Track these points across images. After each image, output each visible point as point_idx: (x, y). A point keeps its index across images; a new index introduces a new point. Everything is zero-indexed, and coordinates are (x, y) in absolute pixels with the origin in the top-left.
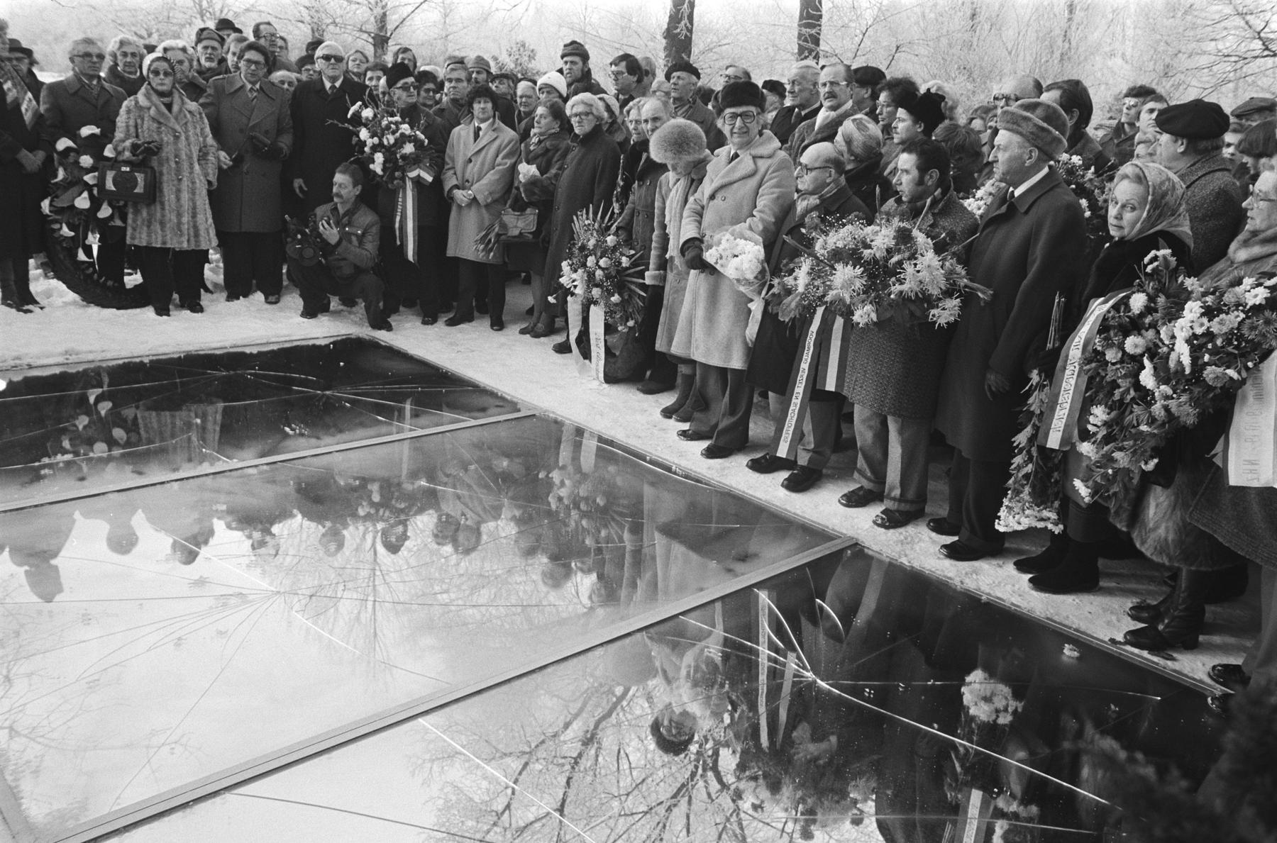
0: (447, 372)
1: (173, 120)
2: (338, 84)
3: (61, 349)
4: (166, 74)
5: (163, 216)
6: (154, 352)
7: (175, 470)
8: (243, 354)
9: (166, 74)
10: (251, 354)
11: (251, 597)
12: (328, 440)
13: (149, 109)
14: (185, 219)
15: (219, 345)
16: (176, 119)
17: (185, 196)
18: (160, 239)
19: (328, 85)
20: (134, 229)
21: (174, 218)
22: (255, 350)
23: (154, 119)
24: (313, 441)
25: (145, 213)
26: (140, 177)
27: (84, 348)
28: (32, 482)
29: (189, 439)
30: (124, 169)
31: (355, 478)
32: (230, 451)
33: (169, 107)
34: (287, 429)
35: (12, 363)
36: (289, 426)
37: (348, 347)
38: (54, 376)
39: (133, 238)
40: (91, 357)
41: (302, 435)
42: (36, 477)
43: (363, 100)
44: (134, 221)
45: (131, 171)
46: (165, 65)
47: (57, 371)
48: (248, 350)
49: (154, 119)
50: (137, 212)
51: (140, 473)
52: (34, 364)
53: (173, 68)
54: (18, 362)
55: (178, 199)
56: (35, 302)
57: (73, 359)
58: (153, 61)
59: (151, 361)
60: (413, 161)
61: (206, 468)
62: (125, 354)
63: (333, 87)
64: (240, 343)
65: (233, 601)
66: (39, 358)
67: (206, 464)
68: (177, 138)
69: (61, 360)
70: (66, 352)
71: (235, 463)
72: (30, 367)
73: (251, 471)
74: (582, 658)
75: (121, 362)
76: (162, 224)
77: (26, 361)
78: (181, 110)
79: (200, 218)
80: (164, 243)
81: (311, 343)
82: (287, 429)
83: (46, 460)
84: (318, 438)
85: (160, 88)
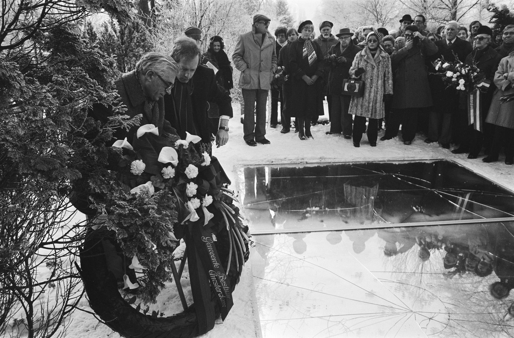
0: (496, 185)
1: (373, 61)
2: (453, 42)
3: (319, 157)
4: (374, 41)
5: (362, 103)
6: (354, 161)
7: (362, 223)
8: (392, 164)
9: (374, 41)
10: (396, 164)
11: (397, 311)
12: (435, 217)
13: (365, 56)
14: (371, 105)
15: (382, 160)
16: (375, 60)
17: (372, 95)
18: (360, 113)
19: (448, 42)
20: (351, 108)
21: (367, 104)
22: (397, 163)
23: (365, 61)
24: (427, 217)
25: (356, 101)
26: (357, 85)
27: (328, 156)
28: (302, 219)
29: (368, 206)
30: (352, 82)
31: (452, 244)
32: (386, 217)
33: (373, 55)
34: (414, 208)
35: (300, 161)
36: (416, 207)
37: (441, 165)
38: (315, 167)
39: (350, 111)
40: (329, 161)
41: (421, 212)
42: (304, 218)
43: (67, 138)
44: (352, 104)
45: (355, 83)
46: (374, 37)
47: (316, 165)
48: (394, 163)
49: (365, 61)
50: (353, 100)
51: (346, 222)
52: (308, 162)
53: (377, 38)
54: (303, 161)
55: (369, 95)
56: (311, 136)
57: (323, 161)
58: (370, 36)
59: (353, 165)
60: (478, 79)
61: (375, 225)
62: (343, 160)
63: (450, 43)
64: (391, 159)
65: (387, 311)
66: (310, 159)
67: (376, 222)
68: (373, 69)
69: (318, 161)
70: (321, 158)
71: (388, 224)
72: (307, 163)
73: (398, 230)
74: (455, 226)
75: (341, 164)
76: (362, 106)
77: (305, 161)
78: (378, 56)
79: (378, 105)
80: (361, 114)
81: (423, 162)
82: (414, 208)
83: (308, 209)
84: (430, 216)
85: (371, 47)
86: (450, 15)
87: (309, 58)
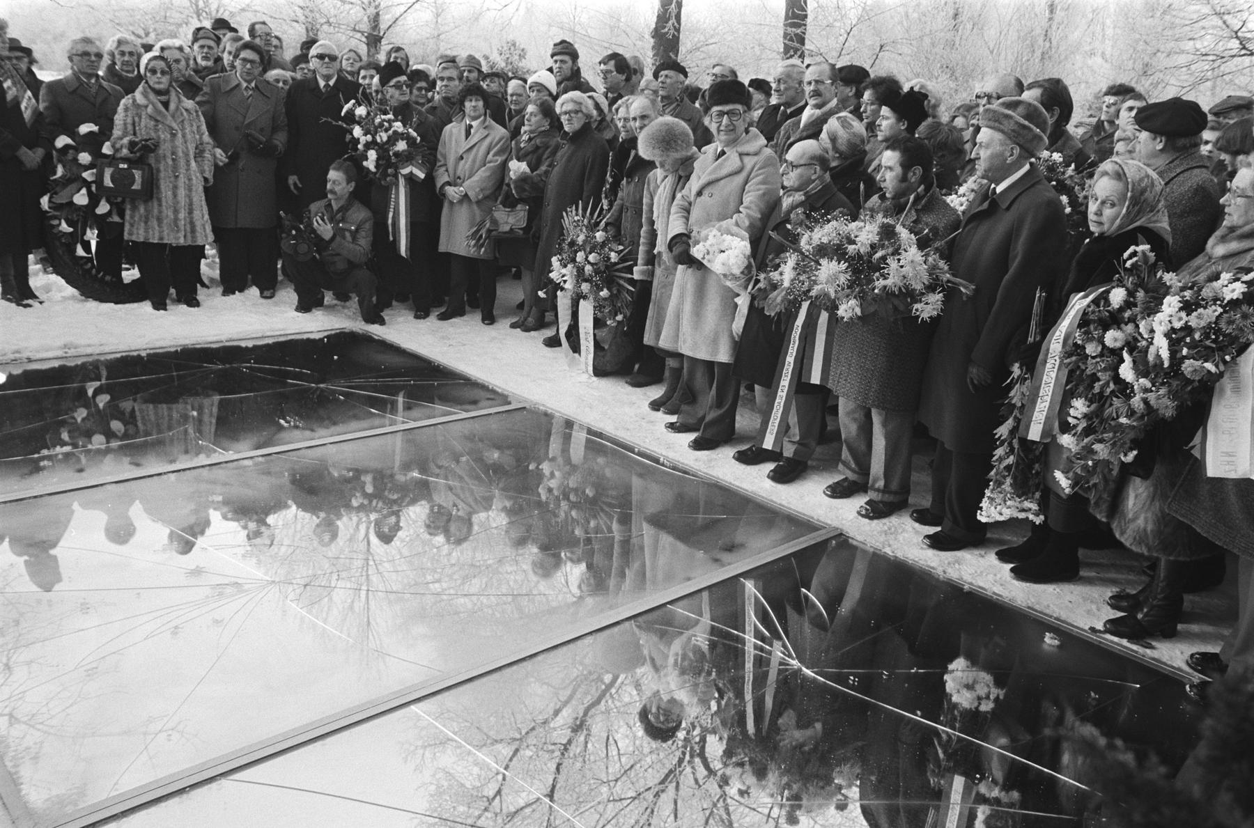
0: (439, 366)
1: (170, 118)
2: (331, 83)
3: (60, 343)
4: (163, 73)
5: (160, 212)
6: (151, 346)
7: (172, 461)
8: (239, 347)
9: (163, 73)
10: (247, 348)
11: (246, 587)
12: (322, 432)
13: (146, 107)
14: (182, 215)
15: (215, 339)
16: (173, 117)
17: (182, 192)
18: (157, 235)
19: (322, 83)
20: (132, 225)
21: (171, 214)
22: (250, 344)
23: (151, 117)
24: (308, 433)
25: (142, 210)
26: (137, 174)
27: (83, 342)
28: (31, 473)
29: (186, 431)
31: (349, 470)
32: (226, 443)
33: (166, 105)
34: (282, 422)
35: (12, 356)
36: (284, 419)
37: (342, 341)
38: (53, 369)
39: (131, 234)
40: (89, 351)
41: (296, 427)
42: (36, 469)
44: (132, 217)
46: (162, 64)
47: (56, 364)
48: (243, 344)
49: (151, 117)
50: (134, 208)
51: (138, 465)
52: (33, 358)
53: (169, 67)
54: (17, 355)
55: (175, 195)
56: (34, 297)
57: (72, 352)
58: (150, 60)
59: (148, 355)
61: (202, 460)
62: (122, 347)
63: (327, 86)
64: (235, 337)
65: (229, 590)
66: (38, 351)
67: (202, 456)
68: (174, 135)
69: (60, 353)
70: (65, 346)
71: (231, 455)
72: (30, 360)
73: (246, 463)
74: (571, 646)
75: (118, 355)
76: (159, 220)
77: (25, 355)
78: (177, 108)
79: (197, 214)
80: (161, 239)
81: (305, 337)
82: (282, 422)
83: (45, 452)
84: (312, 430)
85: (157, 86)
86: (366, 19)
87: (23, 106)
